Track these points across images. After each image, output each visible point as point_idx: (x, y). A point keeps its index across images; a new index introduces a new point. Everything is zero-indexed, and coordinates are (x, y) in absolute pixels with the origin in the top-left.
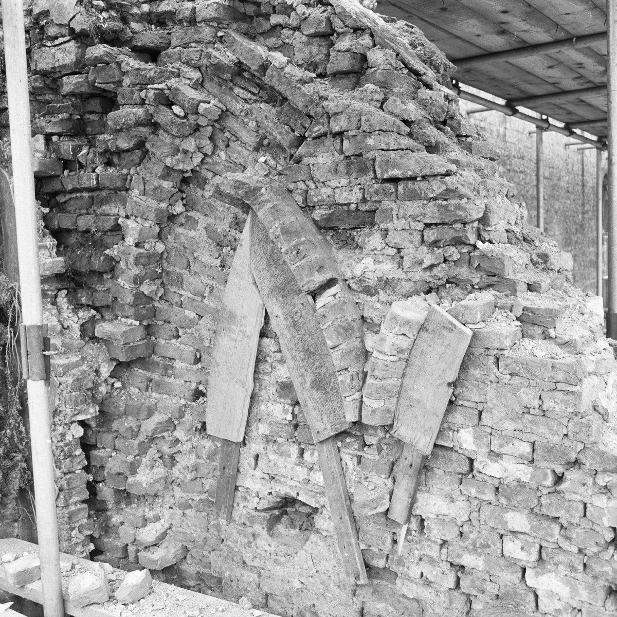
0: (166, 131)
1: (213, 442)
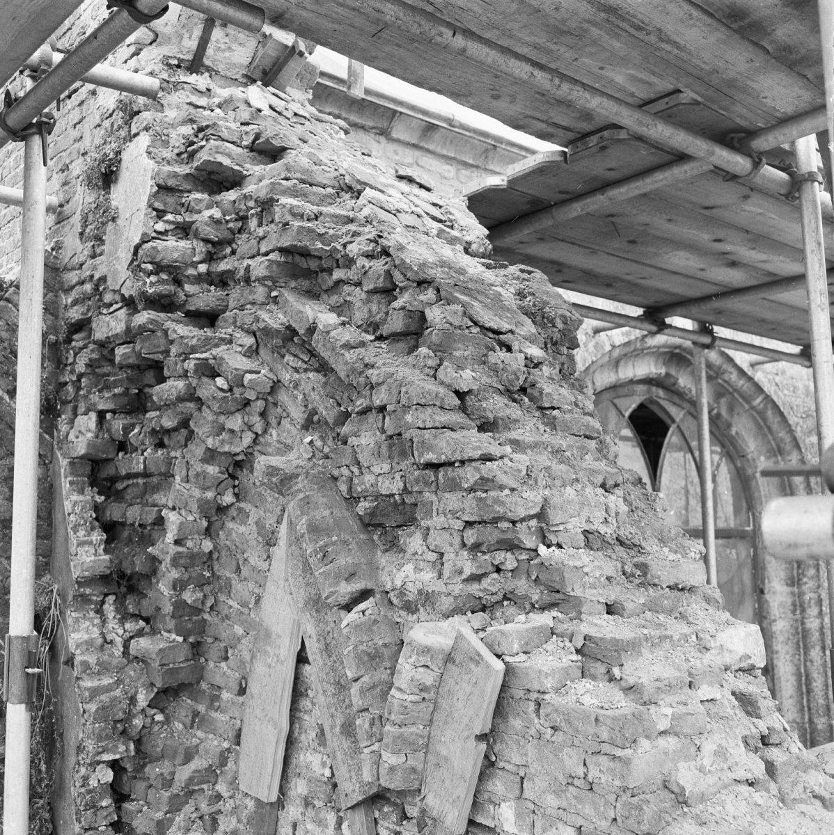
0: (209, 407)
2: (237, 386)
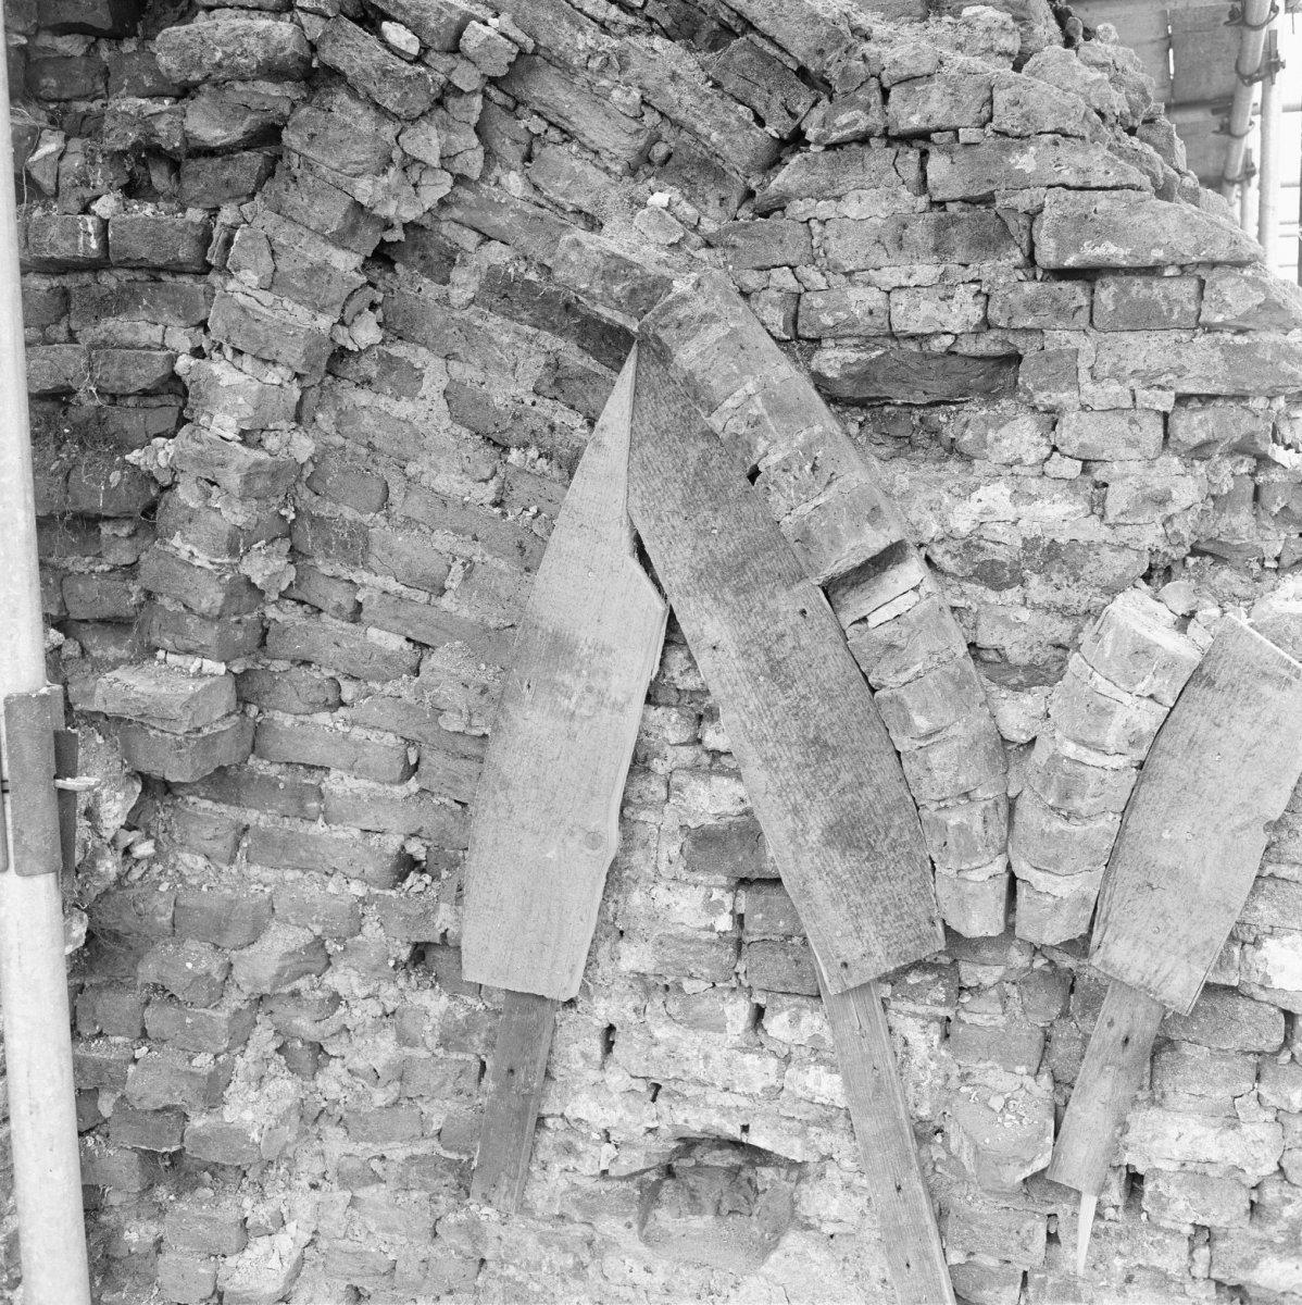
0: (352, 91)
1: (453, 997)
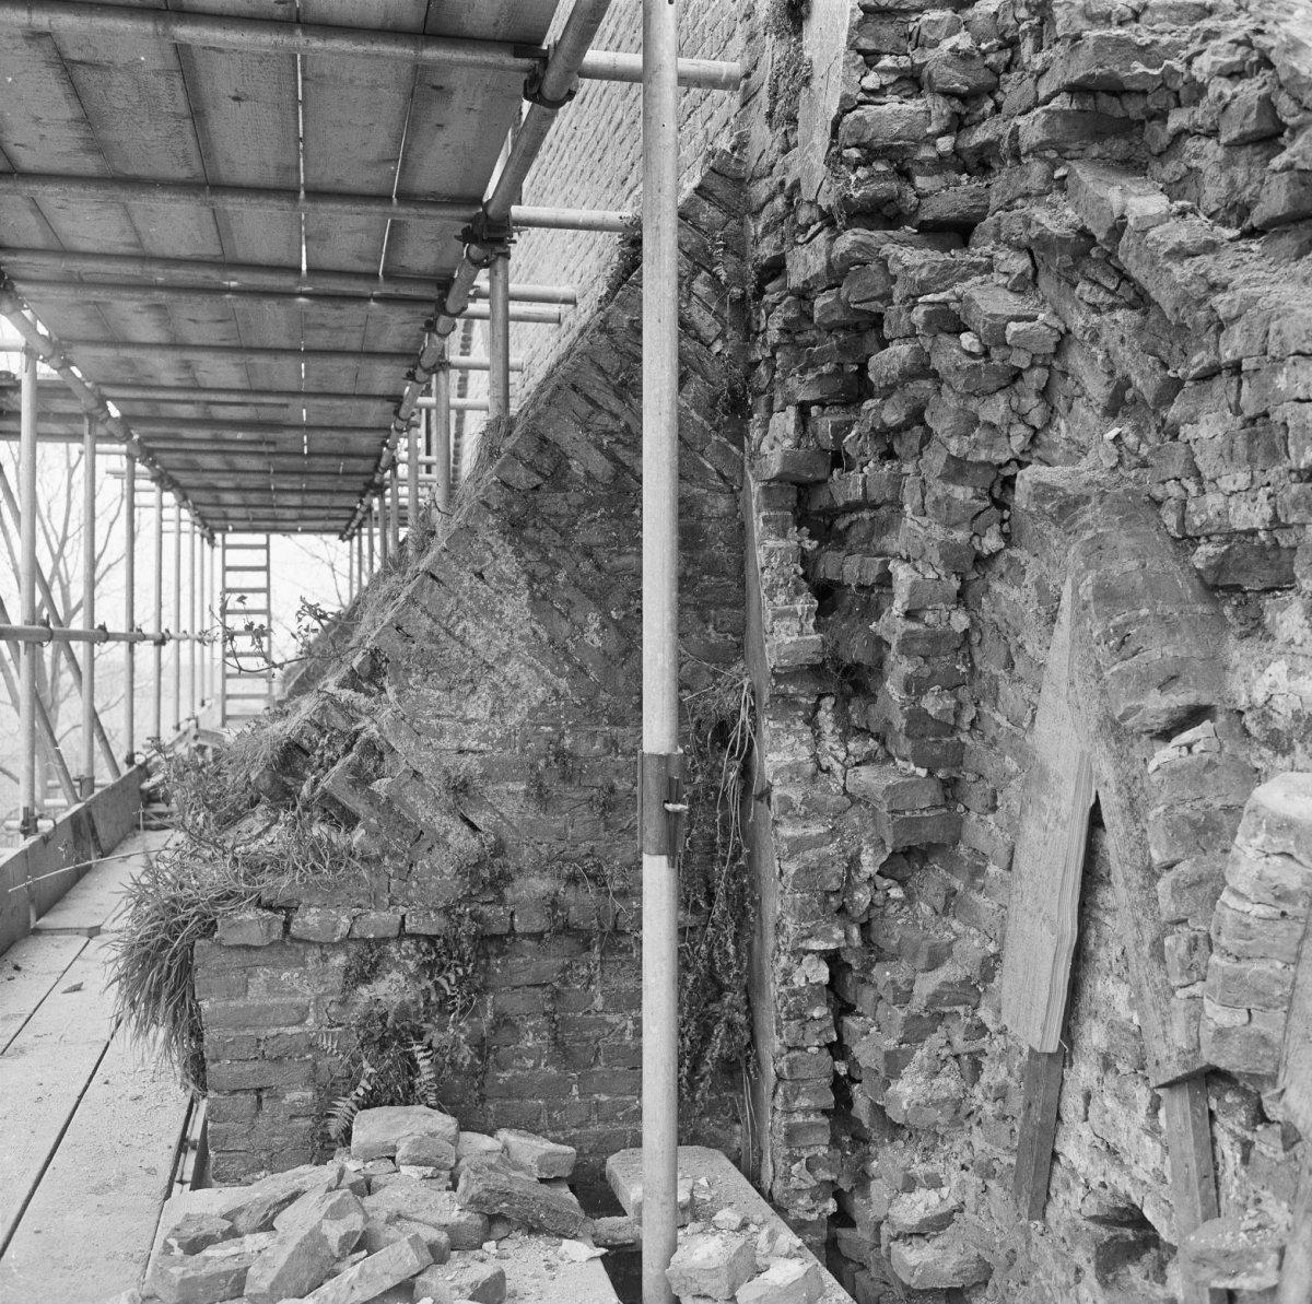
0: (950, 385)
2: (997, 346)
